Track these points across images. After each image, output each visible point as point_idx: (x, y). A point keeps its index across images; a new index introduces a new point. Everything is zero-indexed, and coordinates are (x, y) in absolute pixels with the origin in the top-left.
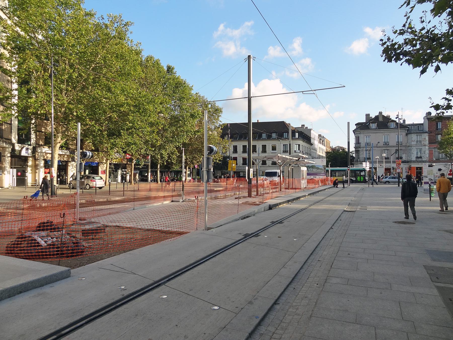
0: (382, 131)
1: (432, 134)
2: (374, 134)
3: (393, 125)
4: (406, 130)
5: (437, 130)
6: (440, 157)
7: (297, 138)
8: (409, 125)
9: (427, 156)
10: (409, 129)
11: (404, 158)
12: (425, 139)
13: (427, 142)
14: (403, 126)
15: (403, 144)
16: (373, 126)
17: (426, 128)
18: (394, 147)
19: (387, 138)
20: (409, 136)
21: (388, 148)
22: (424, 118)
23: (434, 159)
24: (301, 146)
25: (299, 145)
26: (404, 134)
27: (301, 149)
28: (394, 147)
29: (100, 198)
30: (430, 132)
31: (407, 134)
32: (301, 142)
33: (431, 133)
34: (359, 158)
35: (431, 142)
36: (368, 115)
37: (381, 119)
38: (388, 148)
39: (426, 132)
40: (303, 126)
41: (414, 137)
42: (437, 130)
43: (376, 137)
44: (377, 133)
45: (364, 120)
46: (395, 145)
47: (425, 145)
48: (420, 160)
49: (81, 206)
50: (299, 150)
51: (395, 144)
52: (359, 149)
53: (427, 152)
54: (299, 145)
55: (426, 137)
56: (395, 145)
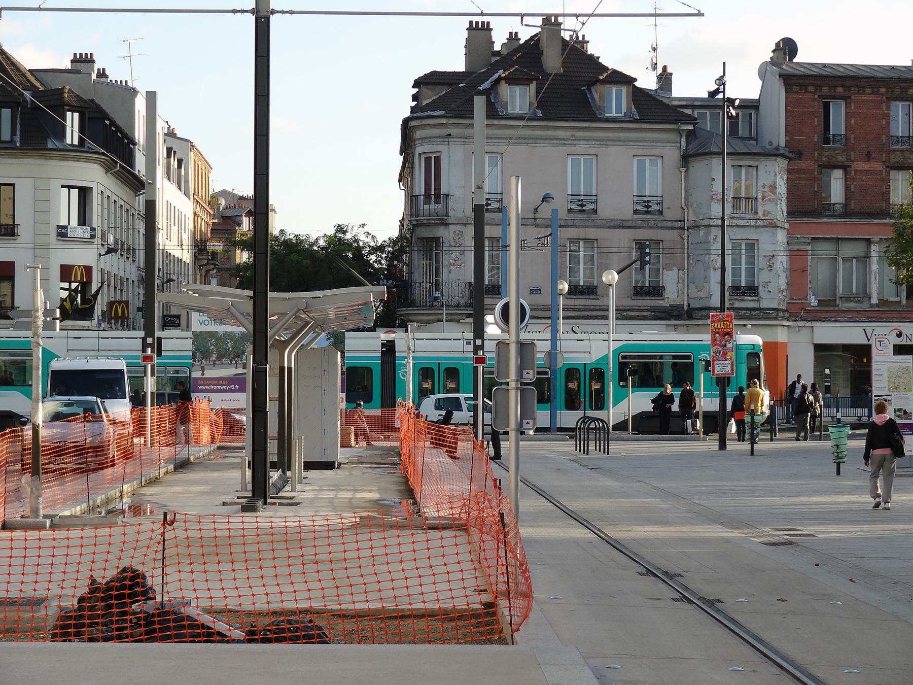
0: (562, 129)
1: (803, 164)
2: (522, 149)
3: (616, 102)
4: (679, 131)
5: (827, 141)
6: (840, 291)
7: (72, 149)
8: (692, 103)
9: (783, 282)
10: (693, 127)
11: (672, 294)
12: (773, 188)
13: (779, 209)
14: (654, 108)
15: (668, 215)
16: (518, 98)
17: (775, 126)
18: (621, 225)
19: (588, 176)
20: (698, 167)
21: (592, 233)
22: (763, 72)
23: (814, 302)
24: (96, 199)
25: (84, 192)
26: (673, 155)
27: (96, 222)
28: (621, 225)
29: (98, 351)
30: (793, 153)
31: (686, 159)
32: (93, 174)
33: (800, 155)
34: (438, 285)
35: (805, 205)
36: (479, 33)
37: (553, 62)
38: (592, 233)
39: (775, 154)
40: (83, 61)
41: (718, 176)
42: (827, 141)
43: (515, 171)
44: (536, 139)
45: (454, 61)
46: (628, 214)
47: (772, 225)
48: (748, 302)
49: (450, 318)
50: (83, 219)
51: (627, 212)
52: (441, 232)
53: (782, 262)
54: (84, 192)
55: (774, 176)
56: (628, 214)
